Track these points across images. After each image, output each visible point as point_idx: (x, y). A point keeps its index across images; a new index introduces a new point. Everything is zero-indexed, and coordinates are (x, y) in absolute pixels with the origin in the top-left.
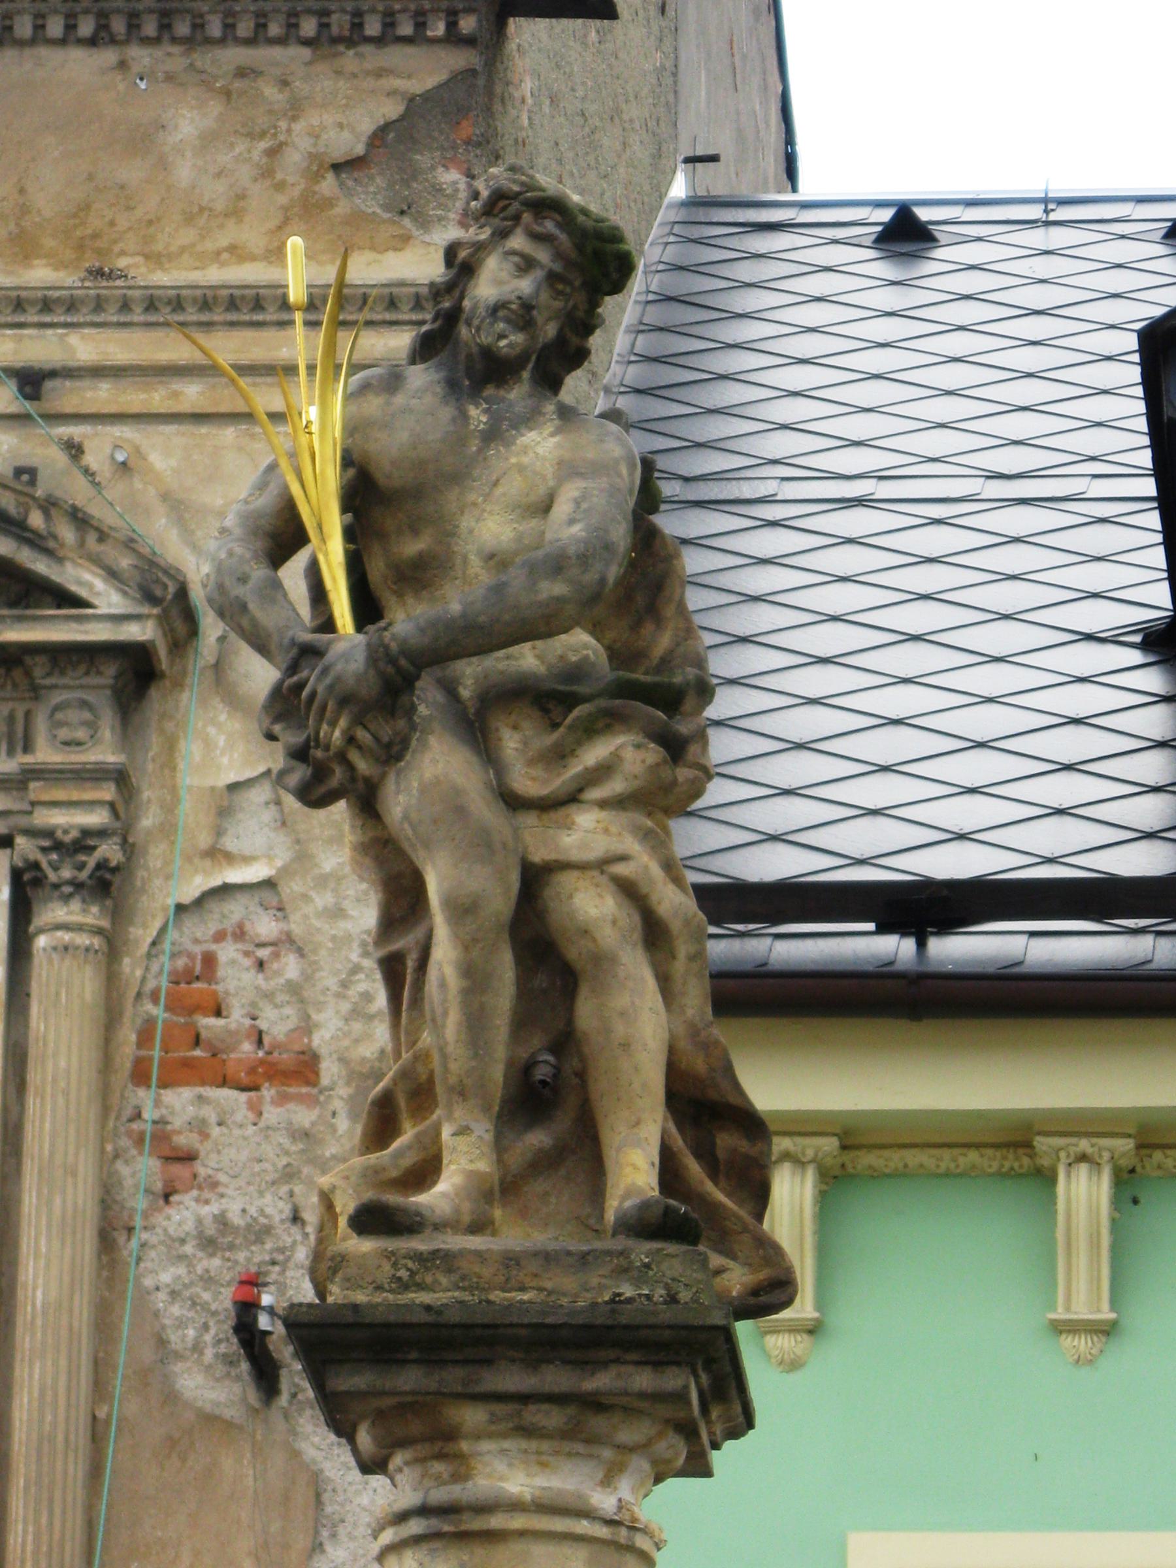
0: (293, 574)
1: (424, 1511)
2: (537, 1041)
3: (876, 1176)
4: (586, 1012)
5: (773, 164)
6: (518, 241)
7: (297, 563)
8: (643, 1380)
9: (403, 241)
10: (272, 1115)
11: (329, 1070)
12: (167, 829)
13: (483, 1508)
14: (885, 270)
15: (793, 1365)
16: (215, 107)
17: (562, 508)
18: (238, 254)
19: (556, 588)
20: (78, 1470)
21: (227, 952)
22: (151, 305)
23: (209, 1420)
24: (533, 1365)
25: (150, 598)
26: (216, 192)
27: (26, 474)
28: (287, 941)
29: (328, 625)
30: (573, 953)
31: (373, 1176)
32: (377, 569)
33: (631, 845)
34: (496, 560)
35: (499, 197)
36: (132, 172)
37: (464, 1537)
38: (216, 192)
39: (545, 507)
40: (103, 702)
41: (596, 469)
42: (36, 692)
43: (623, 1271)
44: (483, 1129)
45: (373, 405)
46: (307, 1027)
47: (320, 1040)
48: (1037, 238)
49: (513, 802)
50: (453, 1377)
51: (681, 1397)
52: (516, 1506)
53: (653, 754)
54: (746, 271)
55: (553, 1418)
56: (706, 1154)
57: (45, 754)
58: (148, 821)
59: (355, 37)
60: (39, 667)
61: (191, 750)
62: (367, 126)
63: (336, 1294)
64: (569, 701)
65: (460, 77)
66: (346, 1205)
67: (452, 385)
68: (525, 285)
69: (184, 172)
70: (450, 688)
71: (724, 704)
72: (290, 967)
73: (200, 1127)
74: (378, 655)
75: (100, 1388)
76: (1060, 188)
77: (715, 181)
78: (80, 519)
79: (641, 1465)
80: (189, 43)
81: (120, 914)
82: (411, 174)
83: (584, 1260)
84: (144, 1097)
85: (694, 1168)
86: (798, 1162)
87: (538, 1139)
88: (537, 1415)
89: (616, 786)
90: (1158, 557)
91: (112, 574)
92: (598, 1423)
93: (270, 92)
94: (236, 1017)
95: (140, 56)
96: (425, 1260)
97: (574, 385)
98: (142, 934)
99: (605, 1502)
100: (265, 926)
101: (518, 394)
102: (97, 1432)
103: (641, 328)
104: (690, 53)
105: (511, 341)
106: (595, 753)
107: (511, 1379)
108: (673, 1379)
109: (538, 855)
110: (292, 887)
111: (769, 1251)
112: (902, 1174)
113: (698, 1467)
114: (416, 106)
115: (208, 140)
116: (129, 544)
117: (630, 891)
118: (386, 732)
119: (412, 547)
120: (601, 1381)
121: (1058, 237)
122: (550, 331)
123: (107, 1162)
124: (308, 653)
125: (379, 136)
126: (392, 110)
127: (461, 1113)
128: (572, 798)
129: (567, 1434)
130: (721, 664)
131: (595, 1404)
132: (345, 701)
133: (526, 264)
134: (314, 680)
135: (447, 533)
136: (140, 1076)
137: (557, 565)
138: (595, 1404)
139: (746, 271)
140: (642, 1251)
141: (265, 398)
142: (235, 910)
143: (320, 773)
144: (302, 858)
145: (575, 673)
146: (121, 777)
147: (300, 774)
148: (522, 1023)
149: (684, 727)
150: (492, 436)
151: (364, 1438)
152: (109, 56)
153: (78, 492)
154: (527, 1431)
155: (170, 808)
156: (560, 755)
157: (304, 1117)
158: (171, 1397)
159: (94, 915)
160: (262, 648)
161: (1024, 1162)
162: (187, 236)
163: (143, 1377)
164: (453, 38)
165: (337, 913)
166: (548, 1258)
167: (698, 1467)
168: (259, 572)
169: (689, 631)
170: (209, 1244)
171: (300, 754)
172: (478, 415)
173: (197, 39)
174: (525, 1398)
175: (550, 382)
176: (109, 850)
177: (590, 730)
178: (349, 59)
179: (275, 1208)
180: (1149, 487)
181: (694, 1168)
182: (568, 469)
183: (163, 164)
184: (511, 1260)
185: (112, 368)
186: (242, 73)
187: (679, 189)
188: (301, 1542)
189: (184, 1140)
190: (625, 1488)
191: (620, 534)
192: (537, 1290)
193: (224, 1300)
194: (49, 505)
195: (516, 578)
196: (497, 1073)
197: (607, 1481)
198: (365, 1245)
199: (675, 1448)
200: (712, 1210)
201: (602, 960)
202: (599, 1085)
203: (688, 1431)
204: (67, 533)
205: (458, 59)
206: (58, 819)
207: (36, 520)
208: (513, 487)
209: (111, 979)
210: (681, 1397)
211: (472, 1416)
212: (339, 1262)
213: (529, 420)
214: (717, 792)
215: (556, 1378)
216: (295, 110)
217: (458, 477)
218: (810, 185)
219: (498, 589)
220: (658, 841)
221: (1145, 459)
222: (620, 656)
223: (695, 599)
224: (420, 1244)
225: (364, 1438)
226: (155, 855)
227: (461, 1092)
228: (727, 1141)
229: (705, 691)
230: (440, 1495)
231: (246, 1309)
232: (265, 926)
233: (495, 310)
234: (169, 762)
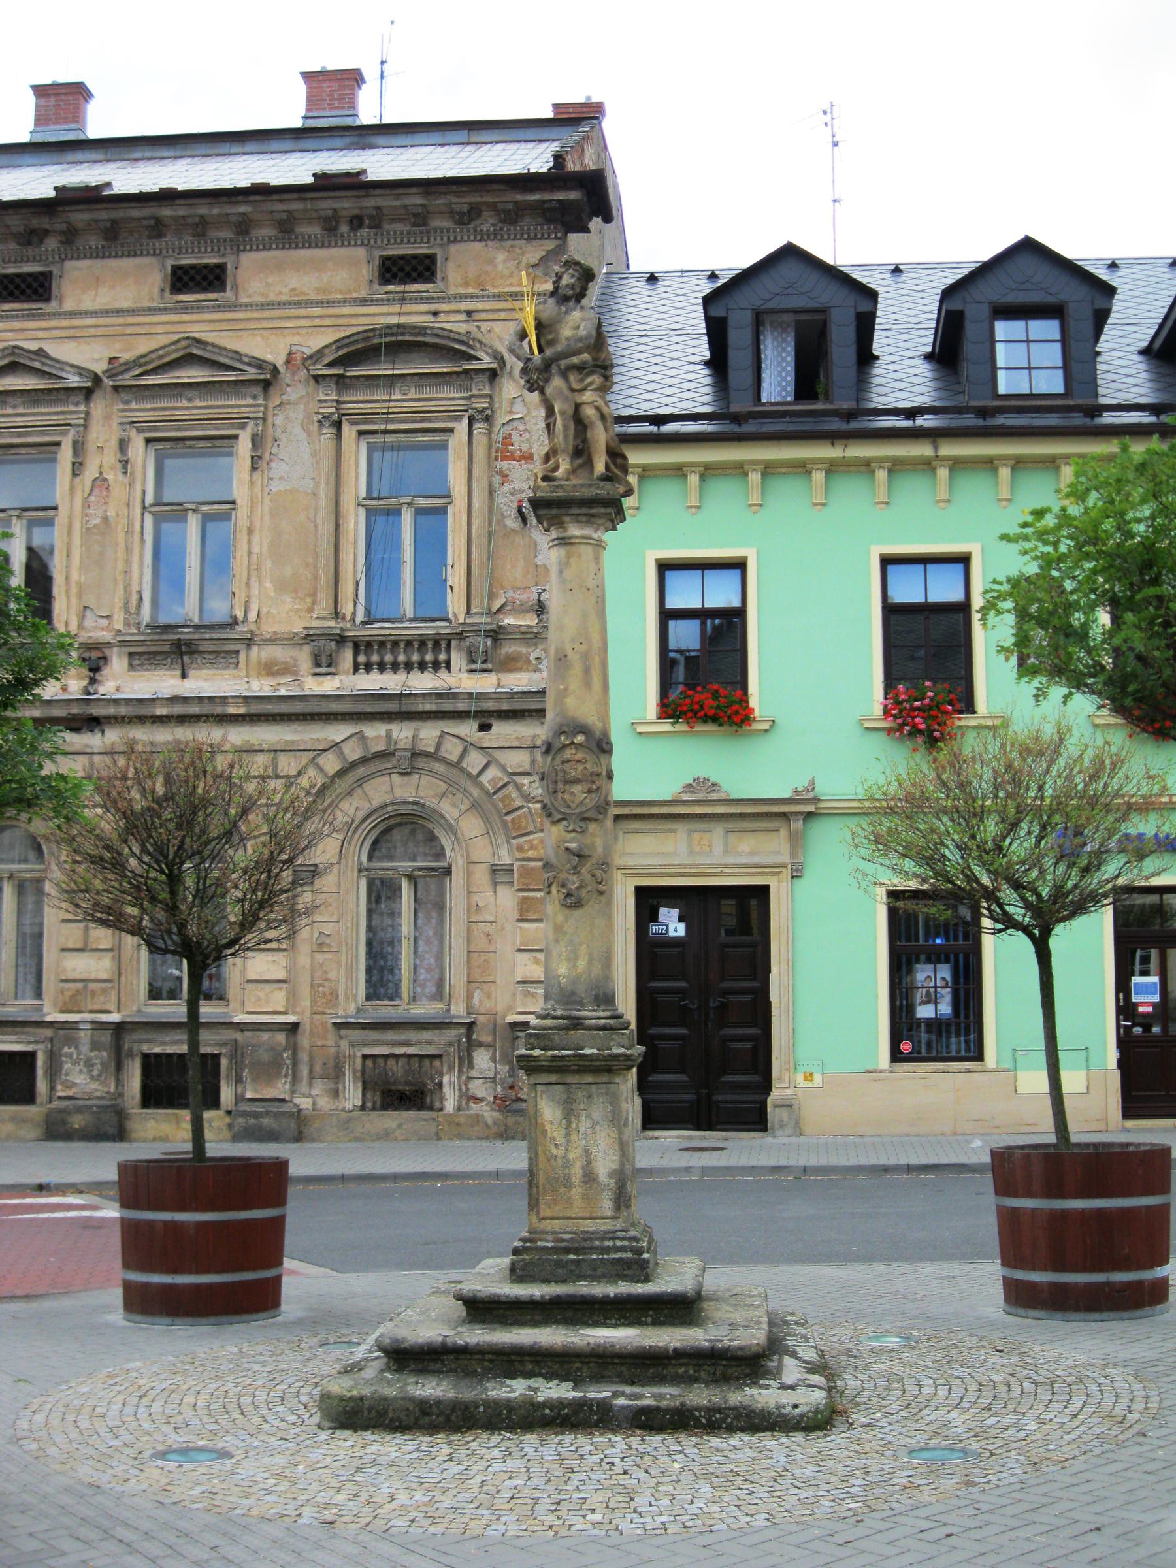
0: (525, 343)
1: (558, 539)
2: (579, 441)
3: (649, 476)
4: (589, 434)
5: (624, 266)
6: (571, 271)
7: (526, 341)
8: (603, 510)
9: (546, 281)
10: (524, 466)
11: (536, 457)
12: (501, 407)
13: (570, 538)
14: (648, 287)
15: (634, 516)
16: (506, 254)
17: (582, 328)
18: (511, 285)
19: (580, 345)
20: (486, 541)
21: (514, 433)
22: (494, 296)
23: (513, 530)
24: (580, 508)
25: (495, 358)
26: (507, 272)
27: (469, 333)
28: (526, 430)
29: (533, 354)
30: (586, 422)
31: (545, 470)
32: (543, 342)
33: (598, 399)
34: (567, 339)
35: (567, 262)
36: (489, 268)
37: (566, 544)
38: (507, 272)
39: (578, 328)
40: (486, 380)
41: (589, 319)
42: (472, 379)
43: (598, 488)
44: (568, 460)
45: (541, 307)
46: (531, 448)
47: (533, 451)
48: (680, 279)
49: (573, 390)
50: (563, 511)
51: (610, 514)
52: (577, 537)
53: (602, 379)
54: (619, 288)
55: (584, 519)
56: (615, 464)
57: (475, 392)
58: (496, 406)
59: (535, 238)
60: (473, 374)
61: (505, 390)
62: (538, 257)
63: (538, 494)
64: (584, 368)
65: (488, 1357)
66: (540, 475)
67: (558, 302)
68: (573, 280)
69: (500, 268)
70: (559, 367)
71: (615, 370)
72: (527, 435)
73: (509, 469)
74: (543, 360)
75: (490, 524)
76: (685, 269)
77: (612, 269)
78: (480, 342)
79: (602, 528)
80: (501, 240)
81: (491, 426)
82: (548, 267)
83: (590, 486)
84: (497, 463)
85: (612, 467)
86: (633, 473)
87: (580, 461)
88: (580, 518)
89: (594, 386)
90: (707, 346)
91: (487, 354)
92: (593, 520)
93: (518, 250)
94: (516, 446)
95: (490, 243)
96: (557, 486)
97: (584, 302)
98: (496, 430)
99: (595, 536)
100: (522, 427)
101: (571, 304)
102: (490, 533)
103: (597, 300)
104: (606, 242)
105: (570, 293)
106: (589, 380)
107: (575, 511)
108: (609, 510)
109: (579, 401)
110: (527, 419)
111: (628, 484)
112: (655, 476)
113: (614, 529)
114: (549, 253)
115: (505, 261)
116: (491, 347)
117: (597, 408)
118: (546, 376)
119: (550, 337)
120: (593, 511)
121: (685, 279)
122: (578, 290)
123: (489, 477)
124: (529, 360)
125: (541, 259)
126: (544, 253)
127: (564, 456)
128: (585, 389)
129: (587, 522)
130: (616, 362)
131: (593, 516)
132: (537, 370)
133: (573, 276)
134: (530, 365)
135: (557, 333)
136: (496, 459)
137: (580, 340)
138: (593, 516)
139: (619, 288)
140: (602, 484)
141: (517, 305)
142: (515, 424)
143: (532, 385)
144: (529, 412)
145: (585, 363)
146: (490, 396)
147: (528, 385)
148: (576, 437)
149: (608, 373)
150: (566, 313)
151: (545, 524)
152: (484, 244)
153: (480, 336)
154: (578, 522)
155: (501, 403)
156: (582, 380)
157: (531, 467)
158: (505, 526)
159: (485, 426)
160: (519, 359)
161: (680, 473)
162: (501, 281)
163: (499, 522)
164: (556, 238)
165: (536, 424)
166: (582, 486)
167: (614, 529)
168: (518, 343)
169: (609, 353)
170: (511, 494)
171: (527, 381)
172: (563, 309)
173: (502, 239)
174: (578, 515)
175: (578, 301)
176: (488, 412)
177: (588, 375)
178: (534, 243)
179: (525, 486)
180: (705, 331)
181: (612, 467)
182: (583, 320)
183: (495, 266)
184: (574, 486)
185: (432, 1429)
186: (512, 246)
187: (604, 271)
188: (532, 555)
189: (506, 472)
190: (599, 533)
191: (594, 333)
192: (531, 1171)
193: (515, 505)
194: (474, 339)
195: (572, 343)
196: (571, 447)
197: (596, 531)
198: (545, 484)
199: (610, 525)
200: (616, 475)
201: (592, 423)
202: (592, 450)
203: (612, 521)
204: (478, 345)
205: (558, 242)
206: (477, 405)
207: (471, 343)
208: (571, 324)
209: (490, 439)
210: (610, 514)
211: (567, 519)
212: (539, 487)
213: (574, 309)
214: (616, 388)
215: (584, 510)
216: (523, 254)
217: (559, 322)
218: (632, 270)
219: (569, 345)
220: (603, 398)
221: (704, 325)
222: (594, 359)
223: (611, 349)
224: (555, 483)
225: (545, 524)
226: (498, 413)
227: (563, 451)
228: (619, 461)
229: (612, 366)
230: (560, 535)
231: (520, 507)
232: (522, 427)
233: (567, 286)
234: (500, 394)
